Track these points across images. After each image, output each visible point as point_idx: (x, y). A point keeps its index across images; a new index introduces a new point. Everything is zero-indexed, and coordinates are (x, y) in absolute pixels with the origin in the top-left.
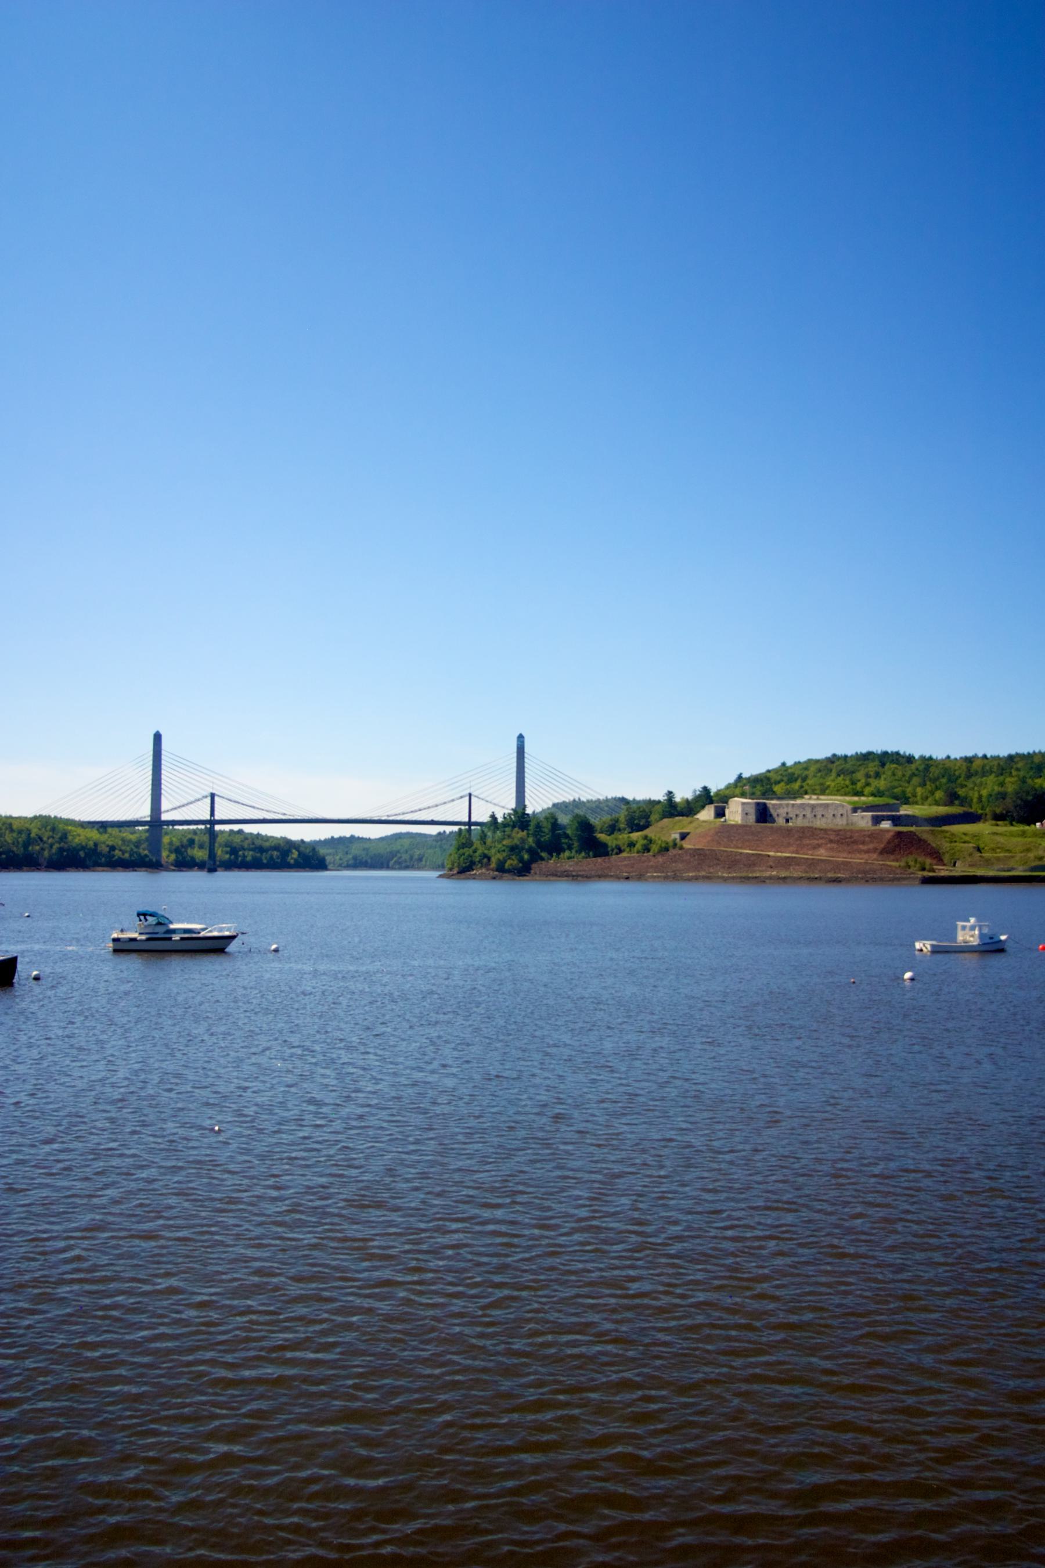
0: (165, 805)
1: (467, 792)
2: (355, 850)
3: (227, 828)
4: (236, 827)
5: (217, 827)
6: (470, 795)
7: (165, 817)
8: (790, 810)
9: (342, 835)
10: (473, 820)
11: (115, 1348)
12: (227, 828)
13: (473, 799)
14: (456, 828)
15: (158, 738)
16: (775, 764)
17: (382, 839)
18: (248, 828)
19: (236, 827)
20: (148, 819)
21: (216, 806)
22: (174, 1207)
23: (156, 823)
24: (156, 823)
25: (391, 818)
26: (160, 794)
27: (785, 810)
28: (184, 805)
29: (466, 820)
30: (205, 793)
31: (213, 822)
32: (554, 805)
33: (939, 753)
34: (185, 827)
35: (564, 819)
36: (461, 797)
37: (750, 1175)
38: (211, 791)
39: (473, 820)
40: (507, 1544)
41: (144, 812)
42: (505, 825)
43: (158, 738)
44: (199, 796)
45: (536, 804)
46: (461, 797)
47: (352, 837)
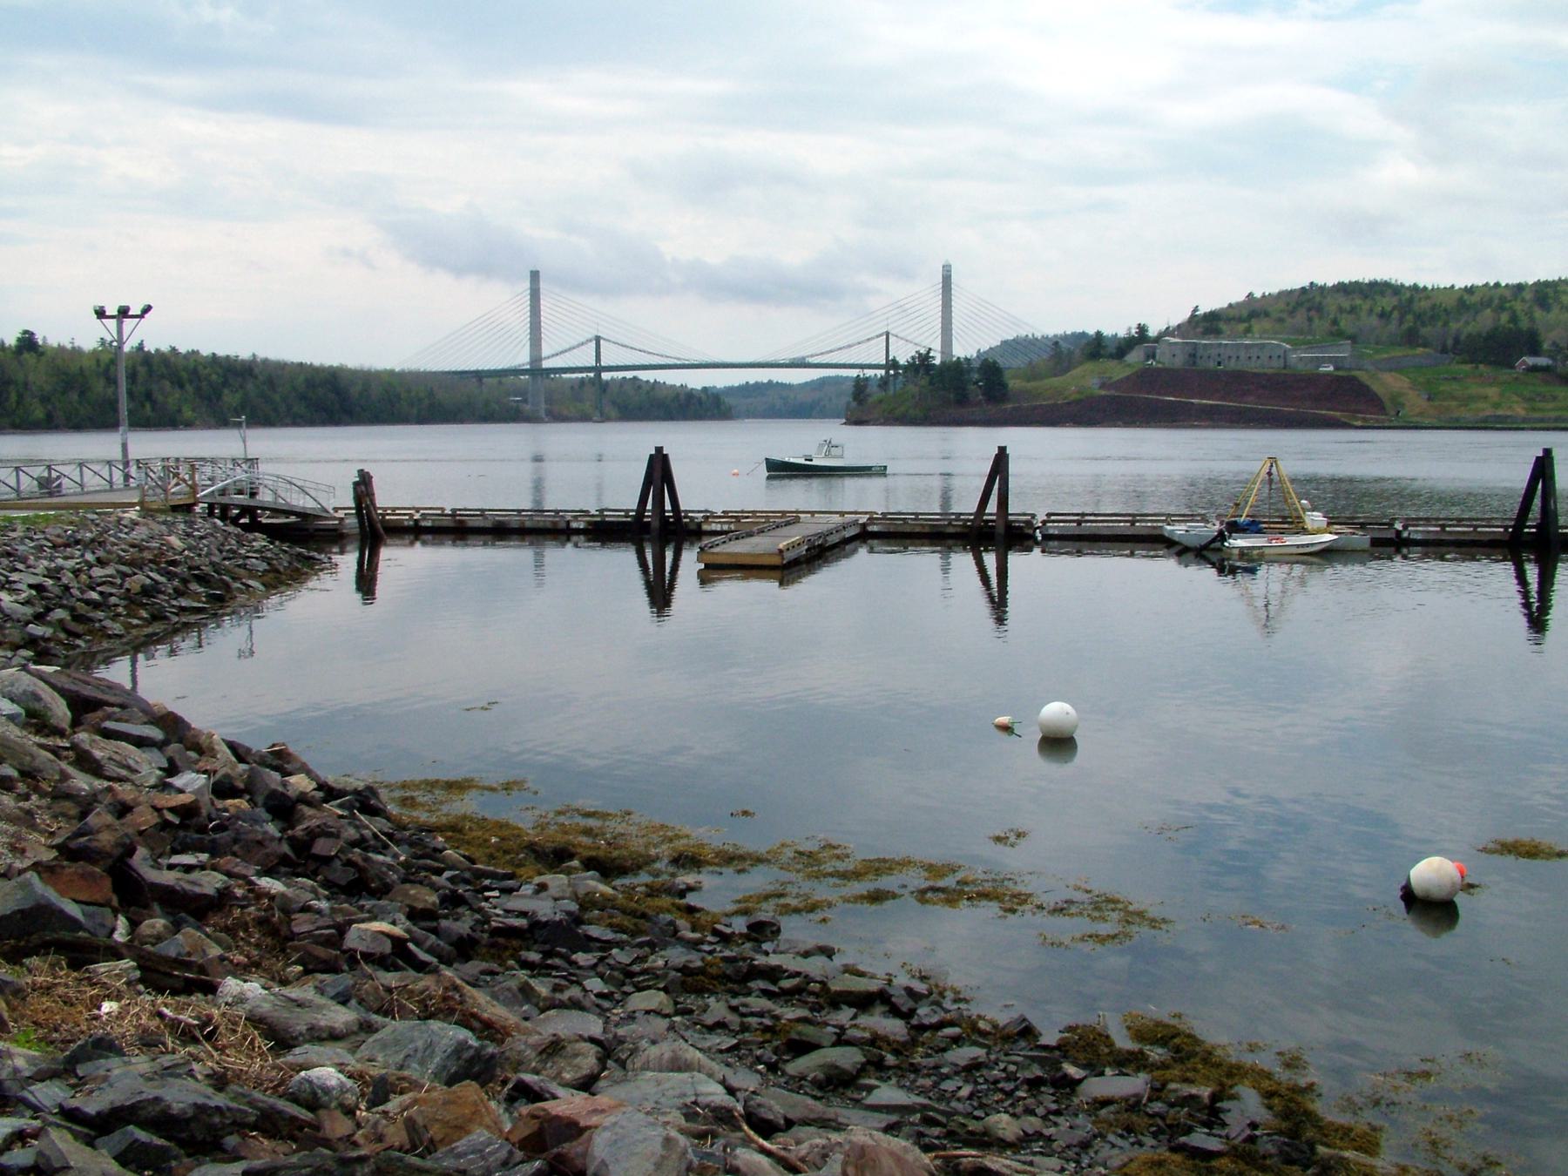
0: (546, 351)
4: (629, 375)
5: (606, 376)
6: (887, 334)
7: (546, 364)
8: (1222, 351)
9: (729, 384)
11: (410, 951)
16: (1239, 297)
18: (644, 376)
19: (629, 375)
22: (1246, 797)
26: (540, 339)
27: (1217, 351)
28: (566, 349)
31: (598, 369)
33: (1426, 280)
34: (574, 376)
40: (143, 1125)
42: (905, 368)
44: (583, 340)
47: (770, 382)
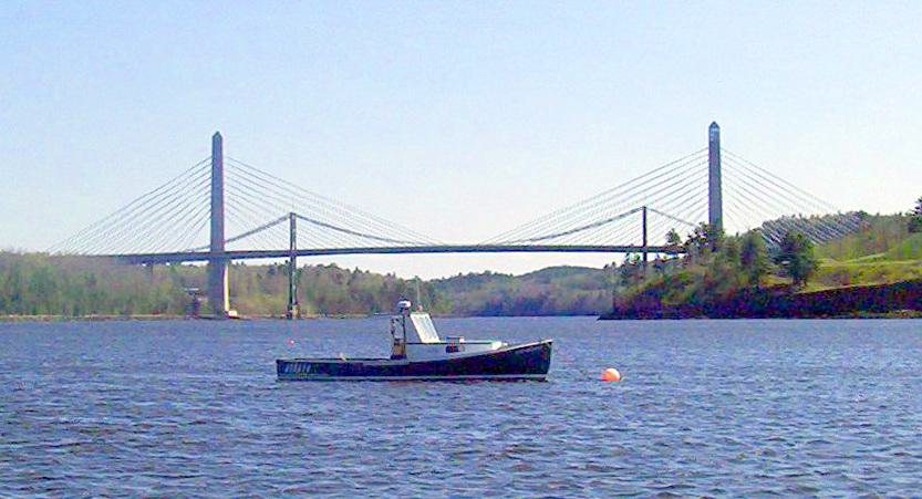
0: (648, 238)
1: (642, 204)
2: (489, 291)
3: (314, 261)
4: (326, 260)
5: (301, 262)
7: (228, 247)
10: (649, 244)
12: (314, 261)
13: (649, 215)
14: (619, 259)
15: (217, 141)
17: (527, 276)
18: (346, 263)
19: (326, 260)
20: (208, 250)
21: (298, 231)
23: (218, 256)
24: (218, 256)
25: (536, 243)
29: (202, 242)
30: (282, 215)
31: (293, 254)
32: (765, 224)
35: (27, 275)
36: (633, 211)
37: (867, 479)
38: (291, 210)
39: (649, 244)
41: (202, 242)
43: (217, 141)
44: (275, 219)
45: (735, 225)
46: (633, 211)
47: (487, 274)
